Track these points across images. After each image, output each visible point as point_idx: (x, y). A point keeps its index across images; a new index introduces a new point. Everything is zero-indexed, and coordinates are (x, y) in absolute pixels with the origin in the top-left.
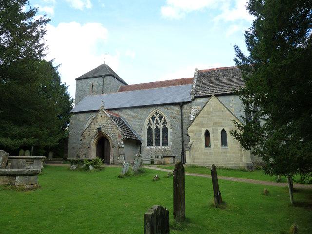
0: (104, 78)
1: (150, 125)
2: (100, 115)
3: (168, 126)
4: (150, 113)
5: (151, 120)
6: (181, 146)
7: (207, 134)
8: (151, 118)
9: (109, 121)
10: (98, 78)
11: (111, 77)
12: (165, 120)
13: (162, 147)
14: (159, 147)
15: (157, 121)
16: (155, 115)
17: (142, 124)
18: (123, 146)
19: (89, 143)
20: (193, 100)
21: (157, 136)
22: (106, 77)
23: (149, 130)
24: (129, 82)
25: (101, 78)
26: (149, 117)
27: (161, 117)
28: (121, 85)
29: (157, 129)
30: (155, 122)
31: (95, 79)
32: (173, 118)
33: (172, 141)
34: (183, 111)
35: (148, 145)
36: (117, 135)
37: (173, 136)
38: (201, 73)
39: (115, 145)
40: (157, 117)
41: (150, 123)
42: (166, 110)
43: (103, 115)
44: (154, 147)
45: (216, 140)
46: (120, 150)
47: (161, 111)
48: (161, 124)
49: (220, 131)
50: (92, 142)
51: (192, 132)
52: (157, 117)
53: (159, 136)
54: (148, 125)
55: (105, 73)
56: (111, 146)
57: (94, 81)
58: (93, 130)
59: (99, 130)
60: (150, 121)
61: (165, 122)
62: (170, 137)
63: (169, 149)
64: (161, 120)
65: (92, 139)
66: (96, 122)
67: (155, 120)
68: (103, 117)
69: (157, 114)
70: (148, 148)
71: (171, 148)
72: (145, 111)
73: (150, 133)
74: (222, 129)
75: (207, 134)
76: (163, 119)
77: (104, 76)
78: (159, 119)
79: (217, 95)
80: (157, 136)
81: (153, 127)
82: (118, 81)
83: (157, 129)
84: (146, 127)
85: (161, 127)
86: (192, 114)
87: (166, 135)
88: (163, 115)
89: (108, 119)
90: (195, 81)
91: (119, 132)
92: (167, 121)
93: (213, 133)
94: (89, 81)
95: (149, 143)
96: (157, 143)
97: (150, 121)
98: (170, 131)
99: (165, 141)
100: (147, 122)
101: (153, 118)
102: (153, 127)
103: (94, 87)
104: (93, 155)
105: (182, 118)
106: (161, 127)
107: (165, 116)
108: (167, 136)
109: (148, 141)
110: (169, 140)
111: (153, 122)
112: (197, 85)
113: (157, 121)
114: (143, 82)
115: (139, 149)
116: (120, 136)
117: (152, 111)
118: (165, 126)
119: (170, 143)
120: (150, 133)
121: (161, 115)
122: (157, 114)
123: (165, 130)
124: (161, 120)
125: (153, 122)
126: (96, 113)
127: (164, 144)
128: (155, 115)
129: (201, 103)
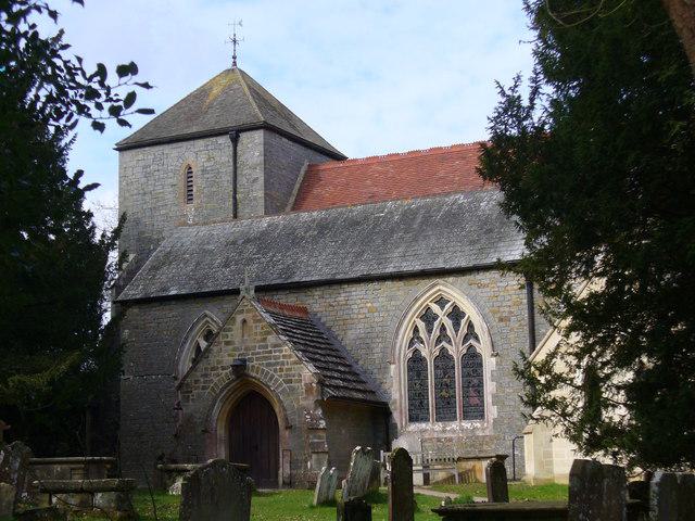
0: (235, 141)
3: (483, 348)
5: (421, 325)
12: (470, 326)
13: (459, 427)
14: (454, 425)
16: (435, 308)
21: (445, 384)
22: (244, 137)
25: (225, 141)
26: (413, 319)
27: (456, 315)
29: (444, 356)
30: (436, 332)
31: (201, 143)
32: (501, 320)
33: (497, 400)
35: (413, 419)
37: (500, 386)
42: (474, 291)
44: (433, 427)
47: (453, 290)
53: (450, 386)
57: (194, 155)
58: (213, 369)
59: (240, 368)
60: (416, 330)
61: (471, 333)
62: (489, 387)
63: (487, 433)
64: (456, 325)
66: (227, 343)
68: (251, 322)
73: (419, 375)
76: (463, 321)
78: (448, 323)
80: (445, 384)
84: (403, 353)
85: (456, 351)
87: (476, 381)
92: (477, 330)
96: (445, 411)
97: (416, 330)
98: (489, 364)
100: (405, 334)
101: (428, 317)
103: (198, 183)
106: (456, 351)
108: (481, 384)
110: (488, 399)
111: (430, 331)
113: (443, 328)
117: (426, 293)
119: (492, 411)
120: (419, 375)
121: (456, 308)
122: (441, 302)
123: (473, 361)
124: (456, 325)
125: (430, 331)
126: (227, 305)
127: (466, 416)
128: (435, 308)
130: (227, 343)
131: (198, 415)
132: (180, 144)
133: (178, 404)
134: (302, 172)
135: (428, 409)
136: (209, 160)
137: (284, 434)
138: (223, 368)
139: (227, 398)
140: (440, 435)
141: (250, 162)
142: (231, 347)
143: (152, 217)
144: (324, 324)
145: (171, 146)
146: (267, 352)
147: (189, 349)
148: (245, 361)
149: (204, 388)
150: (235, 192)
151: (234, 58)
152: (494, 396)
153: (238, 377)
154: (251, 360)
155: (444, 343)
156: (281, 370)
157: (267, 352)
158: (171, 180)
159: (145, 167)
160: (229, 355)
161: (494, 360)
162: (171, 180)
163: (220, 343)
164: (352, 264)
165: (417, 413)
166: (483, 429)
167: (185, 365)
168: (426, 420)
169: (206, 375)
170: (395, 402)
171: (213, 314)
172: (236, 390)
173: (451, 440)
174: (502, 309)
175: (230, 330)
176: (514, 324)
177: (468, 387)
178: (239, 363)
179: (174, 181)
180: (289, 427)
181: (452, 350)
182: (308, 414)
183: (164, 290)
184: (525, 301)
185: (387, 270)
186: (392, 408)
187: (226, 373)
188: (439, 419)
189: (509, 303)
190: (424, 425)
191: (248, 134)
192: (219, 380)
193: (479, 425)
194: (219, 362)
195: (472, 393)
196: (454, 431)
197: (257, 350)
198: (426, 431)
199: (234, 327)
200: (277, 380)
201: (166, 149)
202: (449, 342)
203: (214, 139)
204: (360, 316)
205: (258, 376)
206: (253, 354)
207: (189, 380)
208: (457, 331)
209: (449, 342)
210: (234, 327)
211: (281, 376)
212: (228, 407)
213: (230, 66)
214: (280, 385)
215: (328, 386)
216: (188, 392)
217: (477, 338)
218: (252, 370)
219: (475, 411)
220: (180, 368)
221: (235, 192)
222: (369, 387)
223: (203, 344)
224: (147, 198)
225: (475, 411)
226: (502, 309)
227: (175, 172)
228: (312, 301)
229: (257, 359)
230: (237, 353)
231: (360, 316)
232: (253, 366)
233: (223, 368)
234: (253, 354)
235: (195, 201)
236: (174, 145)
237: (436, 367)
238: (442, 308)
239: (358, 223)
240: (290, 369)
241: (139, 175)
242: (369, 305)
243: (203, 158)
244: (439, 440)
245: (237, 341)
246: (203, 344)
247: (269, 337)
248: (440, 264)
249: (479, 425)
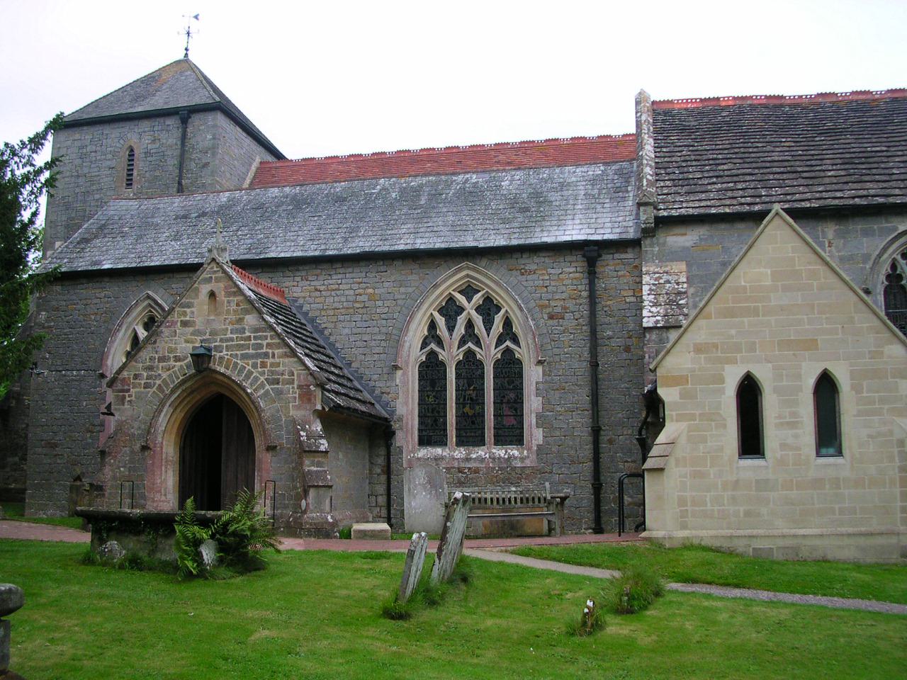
1: (433, 346)
2: (205, 289)
3: (525, 353)
4: (436, 286)
5: (441, 321)
6: (587, 451)
7: (749, 393)
8: (441, 311)
9: (251, 320)
10: (157, 124)
11: (220, 119)
12: (508, 323)
13: (489, 453)
14: (480, 452)
15: (470, 325)
16: (461, 299)
17: (395, 341)
18: (324, 445)
19: (149, 430)
20: (648, 233)
22: (196, 120)
23: (431, 371)
24: (293, 150)
25: (172, 122)
26: (428, 309)
27: (488, 309)
28: (260, 156)
29: (470, 367)
30: (460, 329)
31: (145, 125)
32: (551, 317)
33: (542, 421)
34: (600, 285)
35: (424, 441)
36: (292, 391)
37: (547, 403)
38: (665, 113)
39: (284, 439)
40: (469, 308)
41: (433, 334)
42: (514, 278)
43: (219, 288)
45: (792, 425)
46: (309, 466)
47: (492, 280)
48: (490, 340)
49: (811, 381)
50: (162, 420)
51: (676, 381)
52: (469, 308)
53: (479, 400)
54: (424, 345)
55: (198, 99)
56: (259, 442)
57: (139, 137)
58: (162, 359)
59: (201, 359)
60: (433, 326)
61: (508, 332)
62: (532, 404)
63: (528, 463)
64: (488, 324)
65: (162, 404)
66: (185, 324)
67: (461, 321)
68: (221, 296)
69: (469, 292)
70: (423, 452)
71: (539, 459)
72: (412, 277)
73: (433, 384)
74: (819, 371)
75: (749, 393)
76: (498, 319)
77: (185, 115)
78: (478, 320)
79: (799, 215)
81: (451, 355)
82: (248, 141)
83: (470, 367)
84: (413, 351)
85: (489, 354)
86: (648, 298)
87: (512, 395)
88: (500, 297)
89: (247, 312)
90: (649, 149)
91: (299, 375)
92: (517, 329)
93: (857, 389)
94: (115, 138)
95: (431, 433)
96: (471, 434)
97: (433, 326)
98: (533, 375)
99: (512, 421)
100: (418, 330)
101: (450, 310)
102: (451, 355)
103: (139, 165)
104: (626, 481)
105: (593, 313)
106: (489, 354)
107: (508, 306)
109: (421, 423)
110: (530, 419)
111: (451, 329)
112: (658, 166)
113: (470, 325)
114: (539, 133)
115: (381, 461)
116: (306, 396)
117: (449, 281)
118: (508, 350)
119: (535, 435)
120: (433, 384)
121: (488, 299)
122: (469, 292)
123: (510, 369)
124: (488, 324)
125: (451, 329)
126: (177, 285)
127: (500, 440)
128: (461, 299)
129: (685, 249)
130: (185, 324)
131: (136, 425)
132: (121, 124)
133: (109, 407)
134: (253, 168)
135: (445, 430)
136: (154, 141)
137: (262, 455)
138: (177, 359)
139: (181, 400)
140: (462, 465)
141: (200, 146)
142: (191, 329)
143: (85, 202)
144: (306, 314)
145: (112, 126)
146: (242, 339)
147: (122, 339)
148: (209, 350)
149: (147, 386)
150: (180, 177)
151: (187, 49)
152: (539, 416)
153: (199, 371)
154: (219, 349)
155: (508, 343)
156: (263, 365)
157: (242, 339)
158: (108, 163)
159: (81, 147)
160: (187, 341)
161: (540, 369)
162: (108, 163)
163: (173, 323)
164: (346, 240)
165: (431, 433)
166: (522, 459)
167: (116, 357)
168: (442, 442)
169: (150, 368)
170: (400, 419)
171: (160, 294)
172: (192, 392)
173: (477, 471)
174: (553, 303)
175: (189, 306)
176: (569, 321)
177: (502, 403)
178: (202, 351)
179: (113, 163)
180: (271, 448)
181: (443, 355)
182: (303, 430)
183: (96, 263)
184: (585, 294)
185: (396, 248)
186: (395, 426)
187: (181, 367)
188: (461, 442)
189: (564, 296)
190: (439, 451)
191: (201, 116)
192: (170, 376)
193: (516, 453)
194: (171, 350)
195: (506, 411)
196: (482, 460)
197: (229, 335)
198: (442, 458)
199: (195, 302)
200: (256, 379)
201: (107, 129)
202: (478, 343)
203: (162, 120)
204: (357, 305)
205: (228, 373)
206: (221, 340)
207: (125, 374)
208: (488, 330)
209: (478, 343)
210: (195, 302)
211: (263, 374)
212: (180, 415)
213: (181, 56)
214: (262, 385)
215: (328, 391)
216: (123, 391)
217: (515, 340)
218: (220, 364)
219: (511, 433)
220: (109, 362)
221: (180, 177)
222: (366, 396)
223: (142, 334)
224: (81, 181)
225: (511, 433)
226: (553, 303)
227: (114, 154)
228: (292, 284)
229: (228, 348)
230: (199, 338)
231: (357, 305)
232: (221, 358)
233: (177, 359)
234: (221, 340)
235: (135, 186)
236: (117, 125)
237: (458, 376)
238: (469, 299)
239: (344, 200)
240: (278, 365)
241: (74, 156)
242: (371, 291)
243: (147, 140)
244: (460, 470)
245: (199, 323)
246: (142, 334)
247: (247, 317)
248: (470, 242)
249: (516, 453)
